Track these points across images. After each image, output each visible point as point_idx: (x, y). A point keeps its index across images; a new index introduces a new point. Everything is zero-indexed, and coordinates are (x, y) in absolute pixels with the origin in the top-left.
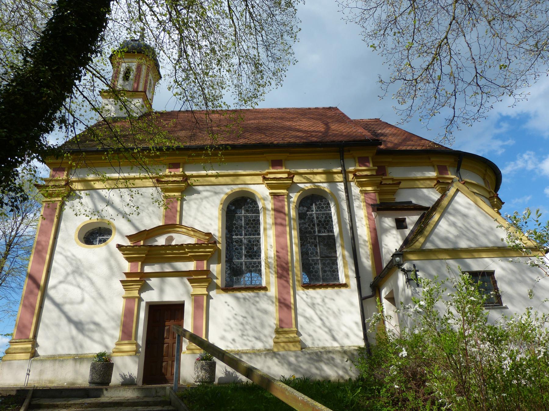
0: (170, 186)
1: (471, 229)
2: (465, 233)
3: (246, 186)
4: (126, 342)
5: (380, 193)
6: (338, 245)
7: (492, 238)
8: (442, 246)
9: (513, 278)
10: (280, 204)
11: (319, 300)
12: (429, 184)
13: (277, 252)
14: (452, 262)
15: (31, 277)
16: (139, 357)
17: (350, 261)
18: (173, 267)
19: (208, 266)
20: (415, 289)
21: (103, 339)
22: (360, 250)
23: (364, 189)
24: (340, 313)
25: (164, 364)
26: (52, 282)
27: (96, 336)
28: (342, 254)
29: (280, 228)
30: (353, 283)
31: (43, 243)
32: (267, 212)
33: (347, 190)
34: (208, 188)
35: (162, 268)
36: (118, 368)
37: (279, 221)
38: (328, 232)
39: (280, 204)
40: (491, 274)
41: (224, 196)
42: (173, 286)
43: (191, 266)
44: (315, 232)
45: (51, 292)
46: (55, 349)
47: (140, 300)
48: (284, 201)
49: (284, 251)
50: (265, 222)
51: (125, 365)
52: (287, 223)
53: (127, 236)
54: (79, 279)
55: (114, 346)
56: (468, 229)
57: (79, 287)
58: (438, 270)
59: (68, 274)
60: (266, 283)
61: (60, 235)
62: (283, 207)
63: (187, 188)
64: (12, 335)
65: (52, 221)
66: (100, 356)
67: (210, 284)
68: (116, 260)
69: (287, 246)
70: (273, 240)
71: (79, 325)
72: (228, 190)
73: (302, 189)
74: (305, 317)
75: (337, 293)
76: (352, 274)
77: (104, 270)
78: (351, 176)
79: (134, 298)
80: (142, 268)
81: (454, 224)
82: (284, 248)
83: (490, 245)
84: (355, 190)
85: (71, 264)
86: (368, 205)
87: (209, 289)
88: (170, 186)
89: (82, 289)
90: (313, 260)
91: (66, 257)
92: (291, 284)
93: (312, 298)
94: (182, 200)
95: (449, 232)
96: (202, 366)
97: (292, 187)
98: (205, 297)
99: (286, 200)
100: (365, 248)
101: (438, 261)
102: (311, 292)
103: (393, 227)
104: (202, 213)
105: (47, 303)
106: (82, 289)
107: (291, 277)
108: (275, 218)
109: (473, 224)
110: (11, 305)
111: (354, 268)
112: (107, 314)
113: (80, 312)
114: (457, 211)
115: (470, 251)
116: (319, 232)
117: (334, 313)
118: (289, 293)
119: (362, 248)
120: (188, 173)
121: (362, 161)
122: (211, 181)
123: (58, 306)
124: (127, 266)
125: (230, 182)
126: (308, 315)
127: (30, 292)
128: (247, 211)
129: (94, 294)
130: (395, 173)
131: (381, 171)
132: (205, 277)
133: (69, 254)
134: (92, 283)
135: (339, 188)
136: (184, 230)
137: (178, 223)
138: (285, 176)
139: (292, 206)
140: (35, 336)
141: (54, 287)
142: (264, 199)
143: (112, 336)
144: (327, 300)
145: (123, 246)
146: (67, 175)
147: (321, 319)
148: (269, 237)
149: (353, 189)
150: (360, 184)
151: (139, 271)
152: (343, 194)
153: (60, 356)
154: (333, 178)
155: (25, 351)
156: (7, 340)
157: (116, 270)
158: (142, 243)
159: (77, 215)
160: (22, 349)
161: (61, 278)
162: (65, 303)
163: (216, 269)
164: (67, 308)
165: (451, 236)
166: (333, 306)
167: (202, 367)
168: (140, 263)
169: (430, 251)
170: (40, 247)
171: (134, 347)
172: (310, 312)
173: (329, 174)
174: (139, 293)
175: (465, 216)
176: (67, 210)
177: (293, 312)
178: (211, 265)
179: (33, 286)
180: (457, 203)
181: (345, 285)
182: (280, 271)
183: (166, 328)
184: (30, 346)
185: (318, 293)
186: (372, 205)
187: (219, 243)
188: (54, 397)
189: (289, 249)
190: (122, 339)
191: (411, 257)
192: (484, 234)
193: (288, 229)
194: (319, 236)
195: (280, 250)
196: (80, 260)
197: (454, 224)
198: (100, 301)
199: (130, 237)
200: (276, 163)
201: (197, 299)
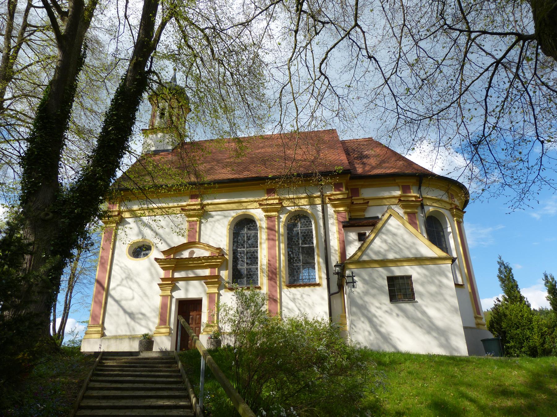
0: (192, 213)
1: (398, 244)
2: (393, 247)
3: (247, 210)
4: (163, 326)
5: (349, 212)
6: (315, 254)
7: (413, 251)
8: (375, 257)
9: (425, 280)
10: (272, 224)
11: (298, 296)
12: (393, 202)
13: (269, 260)
14: (381, 269)
15: (98, 282)
16: (171, 337)
17: (323, 266)
18: (194, 273)
19: (219, 272)
20: (351, 289)
21: (148, 324)
22: (332, 257)
23: (337, 209)
24: (313, 305)
25: (189, 342)
26: (112, 286)
27: (143, 322)
28: (319, 260)
29: (272, 242)
30: (324, 283)
31: (105, 258)
32: (263, 230)
33: (324, 211)
34: (219, 213)
35: (187, 274)
36: (157, 344)
37: (272, 237)
38: (309, 244)
39: (272, 224)
40: (409, 278)
41: (231, 219)
42: (195, 287)
43: (207, 272)
44: (299, 244)
45: (112, 292)
46: (117, 331)
47: (172, 297)
48: (275, 221)
49: (274, 260)
50: (261, 238)
51: (162, 342)
52: (277, 238)
53: (162, 252)
54: (130, 283)
55: (155, 329)
56: (396, 245)
57: (130, 288)
58: (370, 275)
59: (123, 279)
60: (261, 284)
61: (116, 251)
62: (274, 226)
63: (203, 214)
64: (87, 322)
65: (110, 241)
66: (145, 336)
67: (220, 285)
68: (155, 269)
69: (276, 256)
70: (268, 251)
71: (131, 315)
72: (234, 214)
73: (290, 211)
74: (288, 308)
75: (312, 291)
76: (324, 276)
77: (147, 276)
78: (327, 200)
79: (167, 296)
80: (173, 274)
81: (385, 241)
82: (274, 257)
83: (411, 256)
84: (331, 210)
85: (125, 272)
86: (339, 222)
87: (219, 289)
88: (192, 213)
89: (133, 290)
90: (297, 266)
91: (121, 267)
92: (278, 284)
93: (293, 294)
94: (201, 223)
95: (380, 247)
96: (211, 342)
97: (281, 209)
98: (216, 295)
99: (276, 220)
100: (335, 255)
101: (370, 269)
102: (293, 290)
103: (356, 240)
104: (215, 232)
105: (110, 300)
106: (133, 290)
107: (278, 279)
108: (268, 235)
109: (400, 241)
110: (85, 299)
111: (325, 272)
112: (150, 307)
113: (132, 306)
114: (388, 231)
115: (396, 262)
116: (302, 244)
117: (309, 305)
118: (276, 291)
119: (333, 256)
120: (205, 202)
121: (337, 186)
122: (221, 208)
123: (117, 302)
124: (162, 274)
125: (236, 208)
126: (290, 307)
127: (98, 293)
128: (249, 229)
129: (141, 293)
130: (367, 193)
131: (354, 192)
132: (217, 280)
133: (123, 265)
134: (139, 286)
135: (318, 209)
136: (202, 246)
137: (197, 241)
138: (277, 201)
139: (281, 224)
140: (103, 323)
141: (114, 289)
142: (261, 220)
143: (154, 323)
144: (304, 296)
145: (159, 259)
146: (119, 206)
147: (299, 310)
148: (264, 249)
149: (329, 209)
150: (334, 206)
151: (171, 277)
152: (320, 214)
153: (120, 336)
154: (314, 201)
155: (97, 332)
156: (85, 325)
157: (155, 276)
158: (172, 256)
159: (130, 233)
160: (95, 331)
161: (118, 283)
162: (122, 300)
163: (225, 274)
164: (123, 303)
165: (382, 250)
166: (309, 301)
167: (211, 343)
168: (171, 271)
169: (365, 262)
170: (103, 261)
171: (168, 330)
172: (291, 305)
173: (309, 197)
174: (171, 293)
175: (394, 235)
176: (119, 232)
177: (279, 304)
178: (221, 272)
179: (100, 288)
180: (390, 225)
181: (319, 285)
182: (270, 275)
183: (191, 317)
184: (100, 329)
185: (299, 291)
186: (342, 222)
187: (227, 255)
188: (114, 356)
189: (277, 258)
190: (160, 324)
191: (351, 266)
192: (408, 248)
193: (277, 243)
194: (303, 248)
195: (271, 259)
196: (130, 270)
197: (385, 241)
198: (145, 299)
199: (164, 252)
200: (270, 191)
201: (210, 296)
